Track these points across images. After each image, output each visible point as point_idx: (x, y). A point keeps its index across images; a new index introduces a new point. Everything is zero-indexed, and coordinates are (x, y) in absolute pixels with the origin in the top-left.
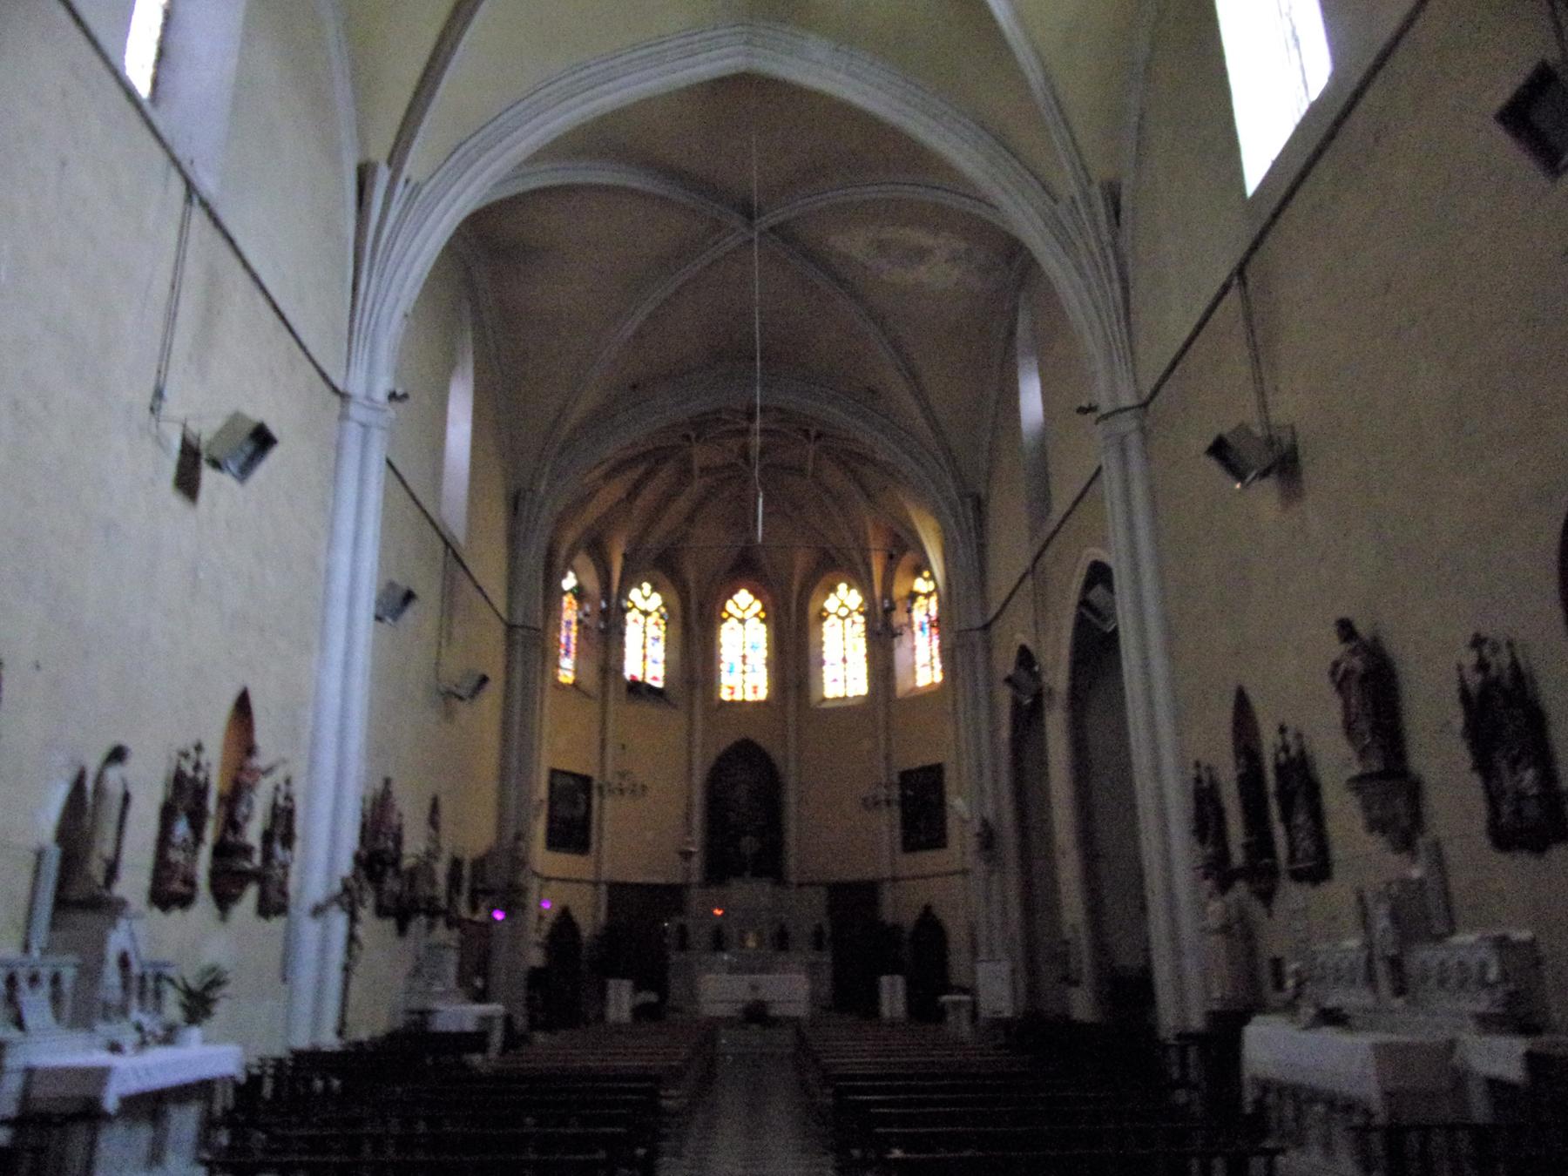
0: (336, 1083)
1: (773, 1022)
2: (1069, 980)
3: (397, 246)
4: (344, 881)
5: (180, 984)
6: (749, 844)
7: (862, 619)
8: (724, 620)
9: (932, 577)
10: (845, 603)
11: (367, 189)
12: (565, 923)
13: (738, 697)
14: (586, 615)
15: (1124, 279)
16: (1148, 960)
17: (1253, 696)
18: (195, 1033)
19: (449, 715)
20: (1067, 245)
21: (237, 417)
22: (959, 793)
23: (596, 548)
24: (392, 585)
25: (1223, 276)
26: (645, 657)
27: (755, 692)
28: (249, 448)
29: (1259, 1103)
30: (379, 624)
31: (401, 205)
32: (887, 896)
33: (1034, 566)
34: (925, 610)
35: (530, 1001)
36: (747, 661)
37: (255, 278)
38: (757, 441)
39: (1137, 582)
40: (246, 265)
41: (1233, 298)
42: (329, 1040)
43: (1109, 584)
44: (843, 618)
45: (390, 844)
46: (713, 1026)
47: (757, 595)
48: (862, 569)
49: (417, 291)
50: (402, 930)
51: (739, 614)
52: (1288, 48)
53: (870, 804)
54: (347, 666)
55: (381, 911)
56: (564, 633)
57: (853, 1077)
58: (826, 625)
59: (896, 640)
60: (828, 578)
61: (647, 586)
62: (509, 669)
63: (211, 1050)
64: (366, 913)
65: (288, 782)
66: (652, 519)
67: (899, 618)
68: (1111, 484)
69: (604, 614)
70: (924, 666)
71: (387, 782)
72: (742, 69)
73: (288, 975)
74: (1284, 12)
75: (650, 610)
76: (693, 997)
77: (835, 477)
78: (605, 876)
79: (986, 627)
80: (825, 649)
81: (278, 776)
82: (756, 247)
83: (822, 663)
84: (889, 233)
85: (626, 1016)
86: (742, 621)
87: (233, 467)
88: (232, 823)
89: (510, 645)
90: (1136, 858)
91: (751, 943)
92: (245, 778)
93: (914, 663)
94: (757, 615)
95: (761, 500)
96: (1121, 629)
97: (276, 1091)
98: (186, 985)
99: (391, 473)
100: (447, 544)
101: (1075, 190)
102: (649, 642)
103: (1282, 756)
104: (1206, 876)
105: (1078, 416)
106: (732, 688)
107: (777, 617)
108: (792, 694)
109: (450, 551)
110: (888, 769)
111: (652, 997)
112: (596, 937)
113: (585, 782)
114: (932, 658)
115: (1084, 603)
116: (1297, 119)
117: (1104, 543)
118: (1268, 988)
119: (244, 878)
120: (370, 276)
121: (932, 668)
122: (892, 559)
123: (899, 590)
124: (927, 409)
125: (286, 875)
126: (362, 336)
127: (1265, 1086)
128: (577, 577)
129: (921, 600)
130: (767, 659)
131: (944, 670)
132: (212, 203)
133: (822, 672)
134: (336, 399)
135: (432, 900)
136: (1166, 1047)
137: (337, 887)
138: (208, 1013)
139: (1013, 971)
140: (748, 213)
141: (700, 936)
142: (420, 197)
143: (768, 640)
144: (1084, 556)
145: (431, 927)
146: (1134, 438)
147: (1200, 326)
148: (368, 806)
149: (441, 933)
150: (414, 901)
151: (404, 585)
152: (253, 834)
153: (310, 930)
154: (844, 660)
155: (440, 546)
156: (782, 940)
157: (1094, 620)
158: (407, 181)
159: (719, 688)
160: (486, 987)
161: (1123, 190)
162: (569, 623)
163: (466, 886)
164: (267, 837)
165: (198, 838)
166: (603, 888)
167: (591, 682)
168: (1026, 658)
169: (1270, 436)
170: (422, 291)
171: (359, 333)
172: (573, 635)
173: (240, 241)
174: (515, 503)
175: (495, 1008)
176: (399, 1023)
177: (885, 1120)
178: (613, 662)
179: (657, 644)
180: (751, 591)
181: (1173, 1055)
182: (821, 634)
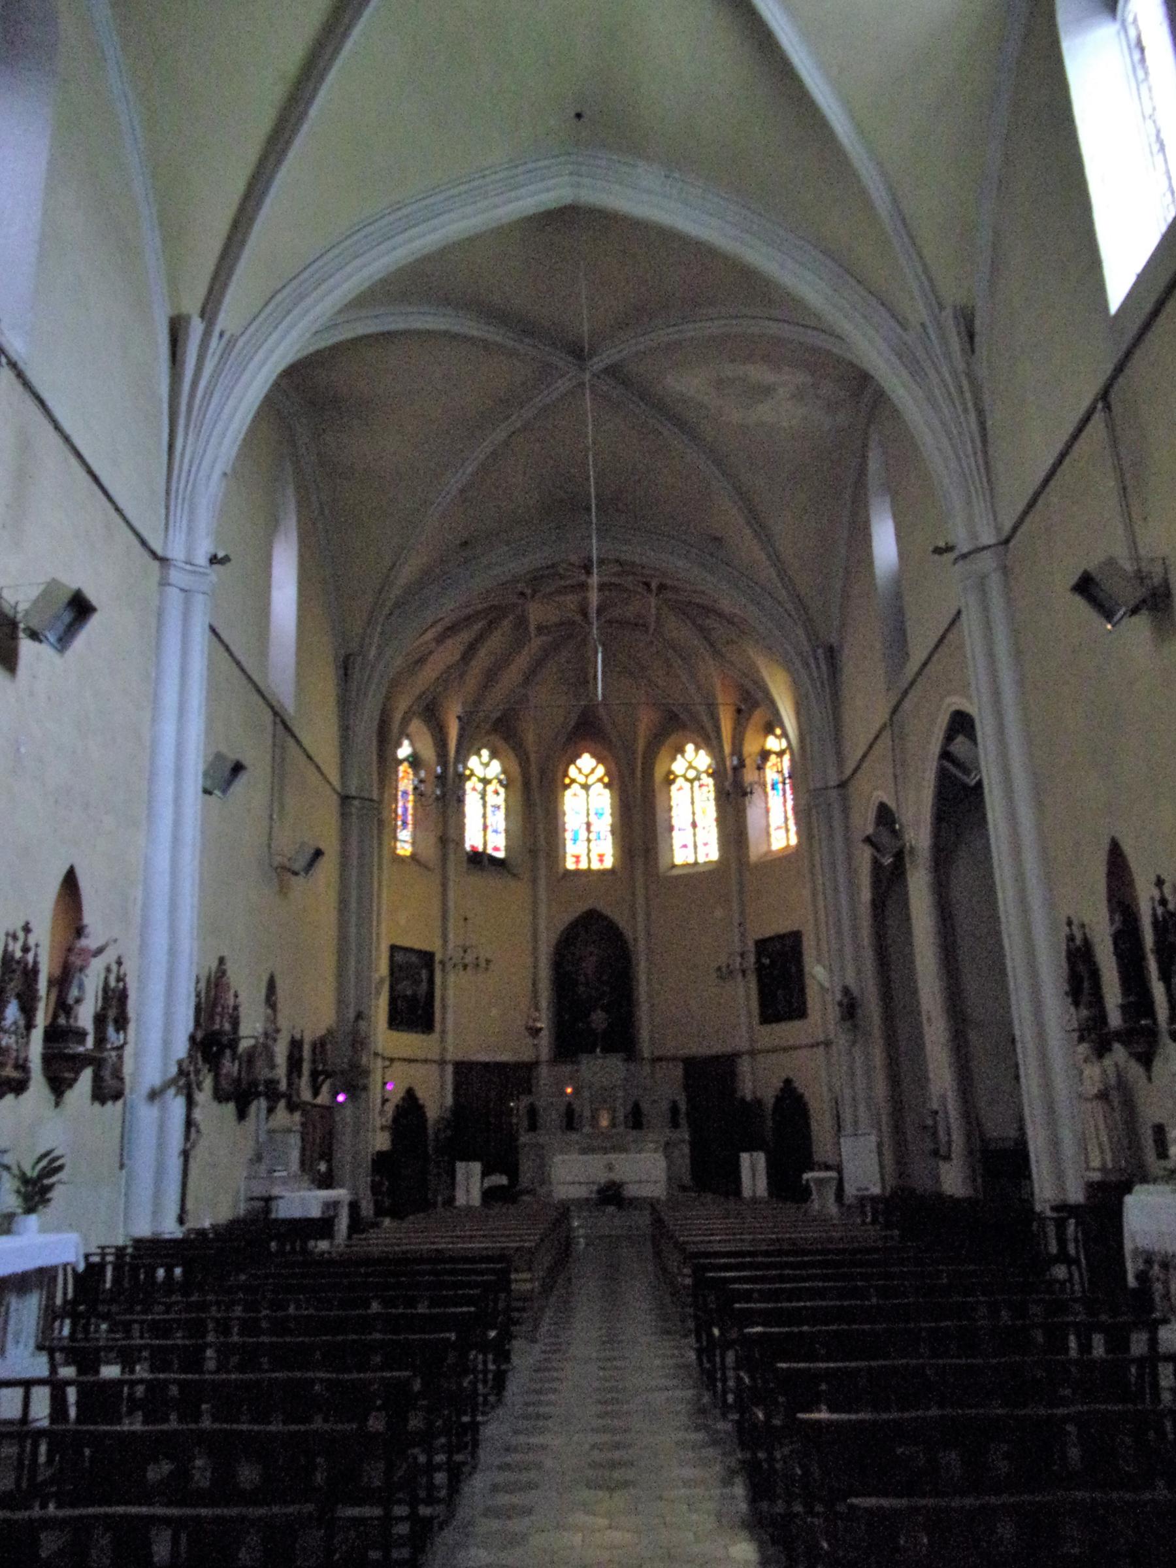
0: (178, 1271)
1: (634, 1203)
2: (939, 1154)
3: (212, 406)
4: (180, 1063)
5: (16, 1171)
6: (599, 1018)
7: (710, 781)
8: (567, 787)
9: (785, 735)
10: (694, 764)
11: (180, 344)
12: (410, 1106)
13: (583, 865)
14: (421, 781)
15: (980, 412)
16: (1022, 1129)
17: (1128, 848)
18: (33, 1220)
19: (283, 890)
20: (915, 369)
21: (53, 586)
22: (819, 961)
23: (431, 714)
24: (219, 757)
25: (1086, 403)
26: (485, 828)
27: (601, 861)
28: (67, 617)
29: (1142, 1277)
30: (207, 796)
31: (216, 358)
32: (744, 1066)
33: (891, 719)
34: (776, 770)
35: (375, 1188)
36: (592, 829)
37: (67, 439)
38: (594, 598)
39: (1001, 729)
40: (57, 427)
41: (1097, 425)
42: (170, 1229)
43: (972, 736)
44: (691, 781)
45: (227, 1027)
46: (565, 1210)
47: (600, 759)
48: (713, 735)
49: (235, 449)
50: (242, 1115)
51: (581, 779)
52: (1151, 153)
53: (725, 974)
54: (176, 840)
55: (220, 1096)
56: (400, 804)
57: (717, 1255)
58: (674, 788)
59: (747, 799)
60: (673, 739)
61: (485, 753)
62: (344, 841)
63: (52, 1237)
64: (204, 1097)
65: (119, 963)
66: (491, 677)
67: (750, 775)
68: (971, 624)
69: (441, 779)
70: (779, 828)
71: (222, 960)
72: (568, 201)
73: (126, 1161)
74: (1147, 114)
75: (489, 777)
76: (544, 1180)
77: (678, 630)
78: (449, 1057)
79: (842, 785)
80: (674, 813)
81: (109, 957)
82: (595, 558)
83: (671, 829)
84: (730, 370)
85: (476, 1199)
86: (586, 787)
87: (52, 639)
88: (63, 1007)
89: (344, 816)
90: (1006, 1024)
91: (604, 1122)
92: (76, 961)
93: (768, 826)
94: (600, 780)
95: (600, 655)
96: (985, 782)
97: (116, 1280)
98: (24, 1174)
99: (215, 639)
100: (276, 714)
101: (924, 315)
102: (489, 809)
103: (1160, 910)
104: (1081, 1039)
105: (936, 557)
106: (577, 857)
107: (621, 777)
108: (639, 862)
109: (278, 720)
110: (743, 941)
111: (503, 1180)
112: (443, 1118)
113: (427, 958)
114: (786, 819)
115: (945, 755)
116: (1163, 228)
117: (964, 690)
118: (1150, 1156)
119: (78, 1062)
120: (186, 434)
121: (787, 830)
122: (741, 715)
123: (751, 748)
124: (776, 560)
125: (120, 1057)
126: (180, 501)
127: (1149, 1259)
128: (412, 744)
129: (773, 759)
130: (612, 826)
131: (798, 833)
132: (21, 365)
133: (671, 838)
134: (156, 564)
135: (272, 1083)
136: (1041, 1218)
137: (174, 1070)
138: (46, 1201)
139: (880, 1145)
140: (578, 353)
141: (552, 1117)
142: (236, 350)
143: (612, 805)
144: (944, 706)
145: (271, 1110)
146: (995, 583)
147: (1063, 456)
148: (203, 985)
149: (282, 1116)
150: (254, 1084)
151: (233, 756)
152: (85, 1017)
153: (147, 1114)
154: (694, 825)
155: (268, 717)
156: (636, 1119)
157: (959, 774)
158: (221, 335)
159: (565, 858)
160: (330, 1169)
161: (978, 314)
162: (405, 793)
163: (306, 1067)
164: (100, 1020)
165: (29, 1026)
166: (450, 1069)
167: (430, 853)
168: (885, 816)
169: (1139, 571)
170: (241, 448)
171: (177, 498)
172: (410, 805)
173: (50, 404)
174: (346, 668)
175: (340, 1194)
176: (242, 1209)
177: (747, 1296)
178: (452, 833)
179: (497, 813)
180: (594, 755)
181: (1051, 1230)
182: (669, 798)
